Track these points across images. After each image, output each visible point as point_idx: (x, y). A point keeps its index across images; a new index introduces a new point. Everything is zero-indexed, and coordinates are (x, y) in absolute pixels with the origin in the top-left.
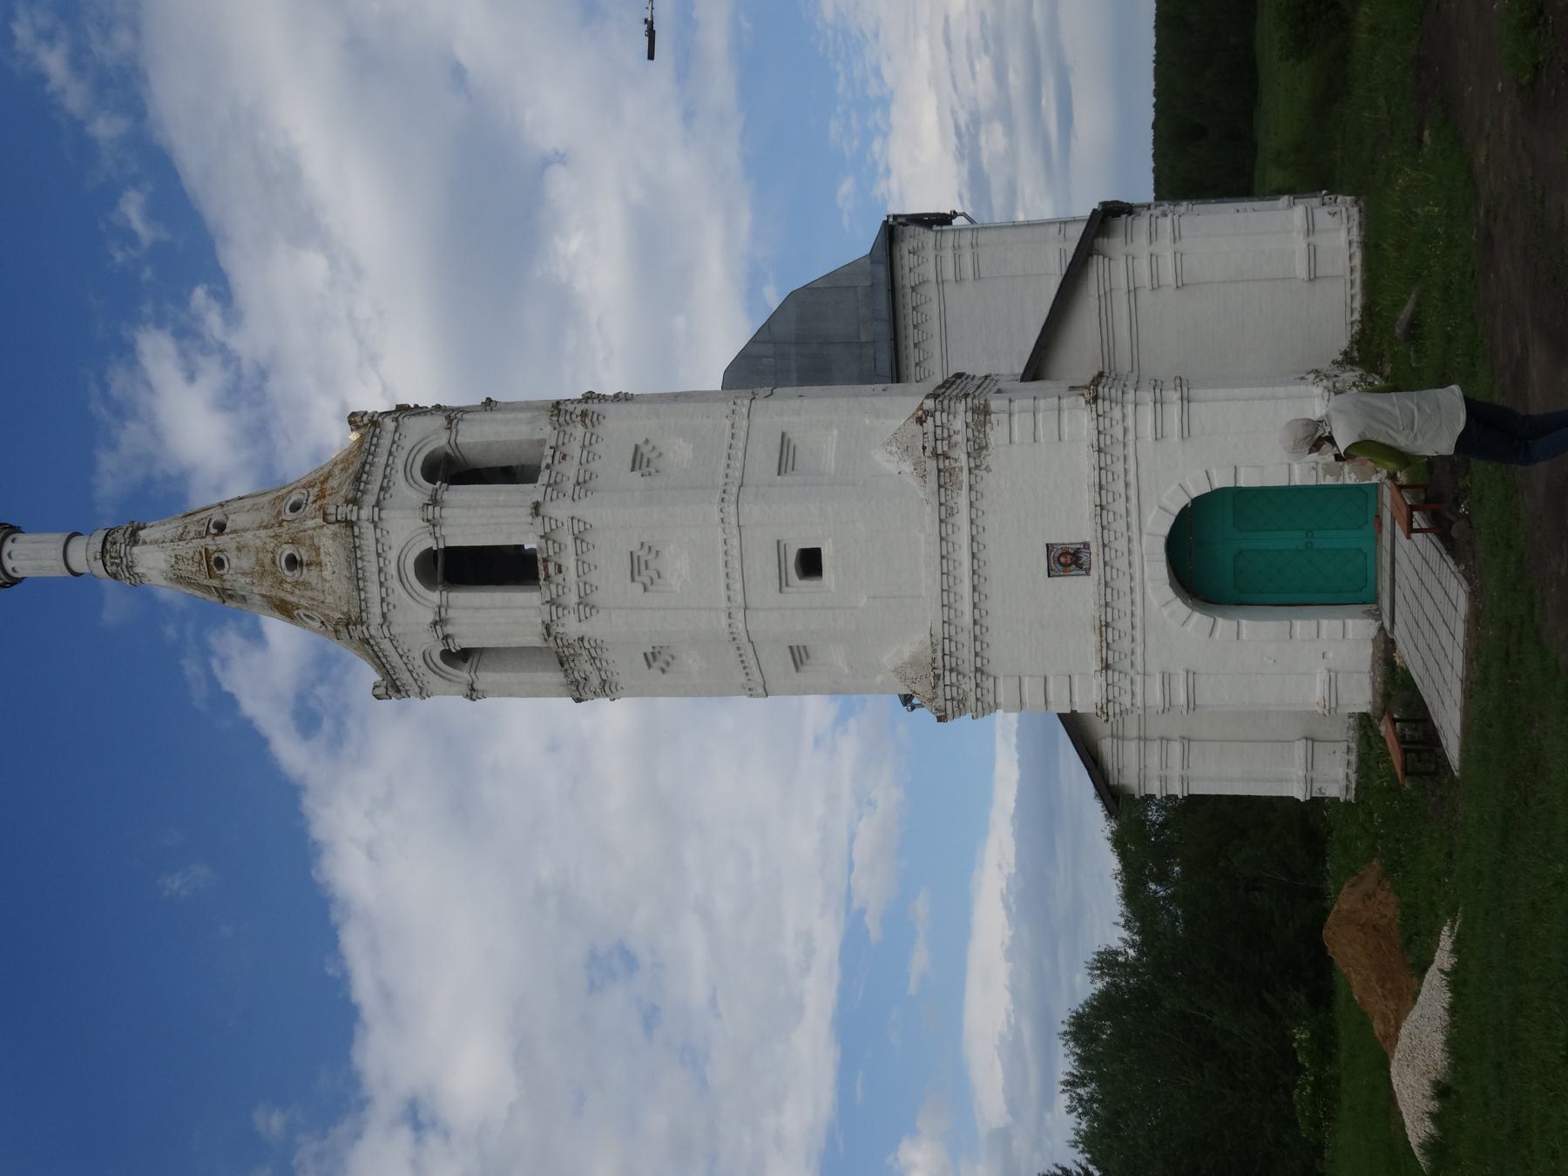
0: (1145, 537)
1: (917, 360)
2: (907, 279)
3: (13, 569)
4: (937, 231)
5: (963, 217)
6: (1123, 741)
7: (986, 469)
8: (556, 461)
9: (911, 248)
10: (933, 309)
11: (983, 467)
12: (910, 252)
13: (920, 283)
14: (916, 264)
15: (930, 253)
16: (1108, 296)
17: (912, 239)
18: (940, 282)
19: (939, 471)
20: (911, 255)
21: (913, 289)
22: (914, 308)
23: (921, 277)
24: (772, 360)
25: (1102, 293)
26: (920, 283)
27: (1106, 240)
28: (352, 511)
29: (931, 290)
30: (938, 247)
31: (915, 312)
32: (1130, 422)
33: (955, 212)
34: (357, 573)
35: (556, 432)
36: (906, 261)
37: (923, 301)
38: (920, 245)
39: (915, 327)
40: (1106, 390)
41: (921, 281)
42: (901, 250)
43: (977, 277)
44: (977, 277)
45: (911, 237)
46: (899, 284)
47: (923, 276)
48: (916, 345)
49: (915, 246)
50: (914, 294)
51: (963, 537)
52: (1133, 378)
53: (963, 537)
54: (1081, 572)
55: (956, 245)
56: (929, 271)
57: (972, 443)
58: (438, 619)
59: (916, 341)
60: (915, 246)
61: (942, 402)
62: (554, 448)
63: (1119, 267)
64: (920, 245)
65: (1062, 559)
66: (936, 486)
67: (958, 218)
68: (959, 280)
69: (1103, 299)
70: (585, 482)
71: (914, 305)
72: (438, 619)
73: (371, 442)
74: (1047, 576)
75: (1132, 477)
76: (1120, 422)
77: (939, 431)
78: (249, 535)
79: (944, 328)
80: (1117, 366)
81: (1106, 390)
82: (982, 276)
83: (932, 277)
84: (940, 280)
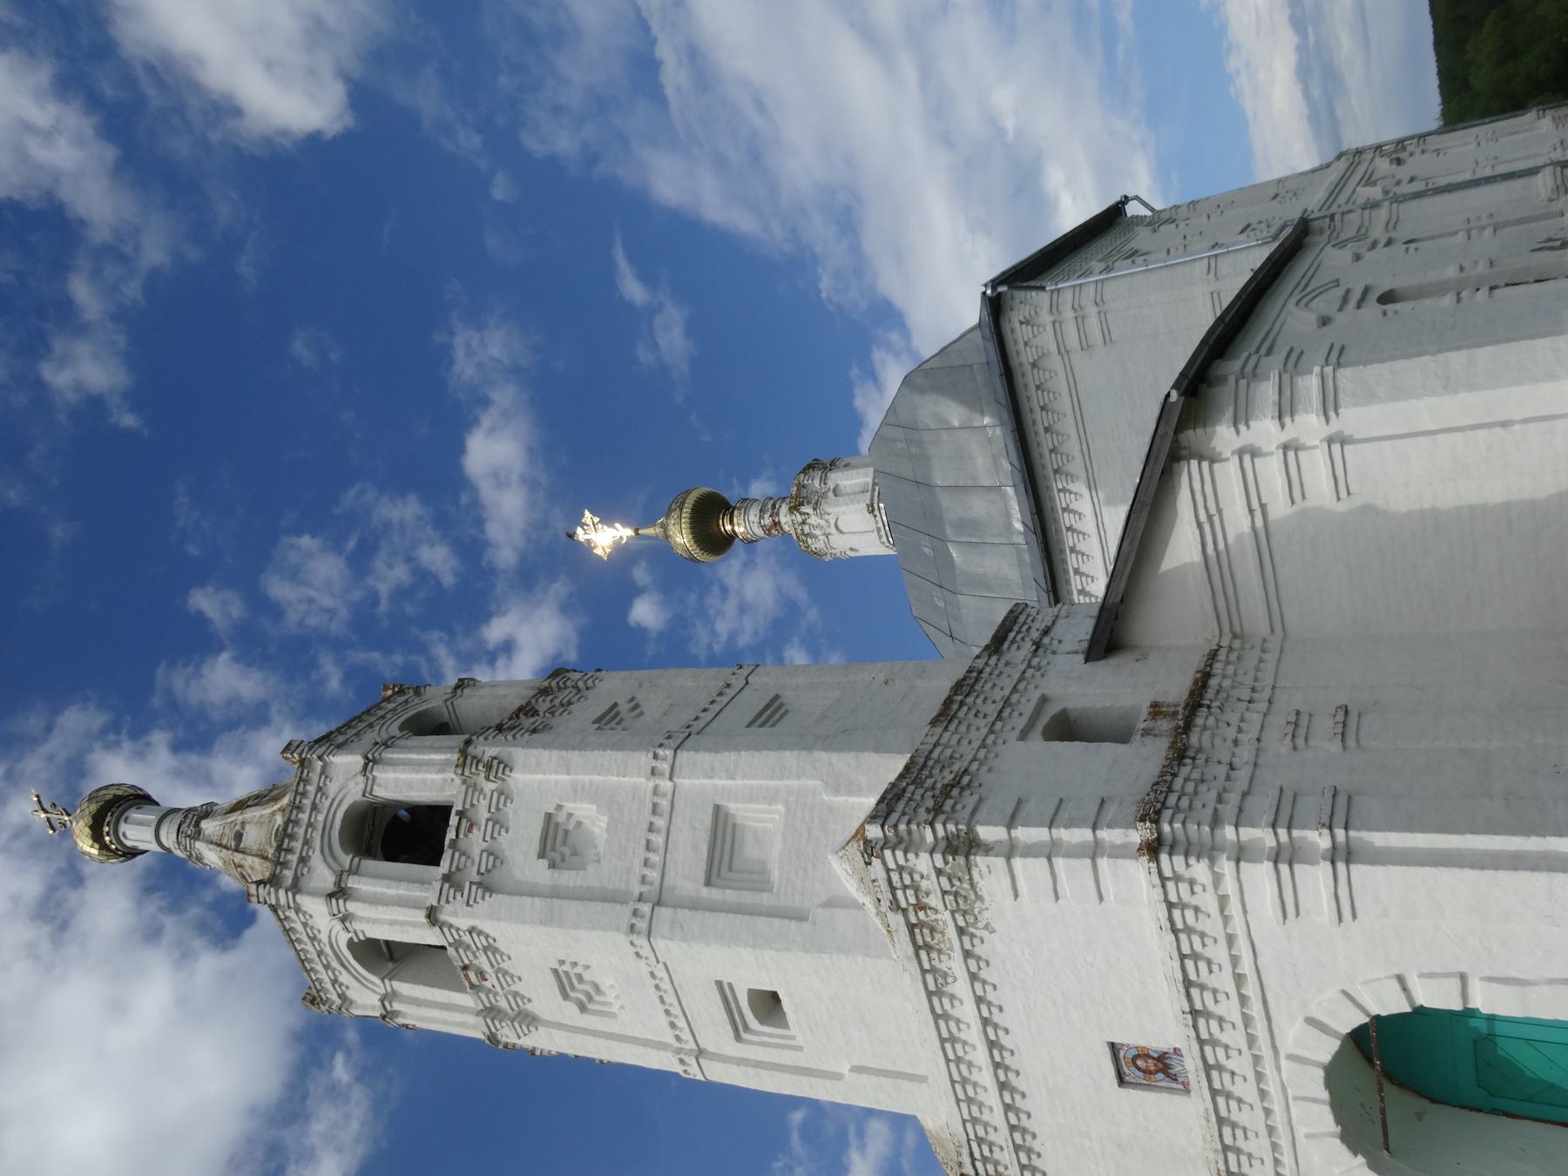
0: (1283, 1062)
1: (1051, 447)
2: (1023, 357)
3: (124, 835)
4: (1052, 291)
5: (1135, 202)
6: (1348, 862)
7: (986, 927)
8: (461, 836)
9: (1022, 318)
10: (1060, 384)
11: (980, 925)
12: (1021, 323)
13: (1039, 357)
14: (1031, 336)
15: (1046, 318)
16: (1216, 520)
17: (1023, 305)
18: (1064, 352)
19: (911, 928)
20: (1024, 326)
21: (1034, 365)
22: (1038, 387)
23: (1039, 350)
24: (904, 444)
25: (1203, 517)
26: (1039, 357)
27: (1200, 431)
28: (269, 893)
29: (1055, 362)
30: (1054, 308)
31: (1039, 392)
32: (1229, 886)
33: (1126, 197)
34: (299, 955)
35: (464, 787)
36: (1018, 335)
37: (1047, 377)
38: (1033, 313)
39: (1043, 408)
40: (1177, 825)
41: (1040, 354)
42: (1010, 322)
43: (1107, 339)
44: (1107, 339)
45: (1021, 303)
46: (1014, 362)
47: (1042, 349)
48: (1047, 430)
49: (1027, 315)
50: (1035, 371)
51: (967, 1011)
52: (1274, 644)
53: (967, 1011)
54: (1174, 1085)
55: (1076, 306)
56: (1047, 340)
57: (952, 898)
58: (385, 1013)
59: (1046, 425)
60: (1027, 315)
61: (895, 826)
62: (461, 814)
63: (1229, 472)
64: (1033, 313)
65: (1140, 1063)
66: (910, 949)
67: (1130, 203)
68: (1086, 346)
69: (1213, 510)
70: (488, 871)
71: (1038, 383)
72: (385, 1013)
73: (296, 791)
74: (1115, 1082)
75: (1246, 967)
76: (1210, 888)
77: (895, 877)
78: (250, 859)
79: (1078, 408)
80: (1246, 626)
81: (1177, 825)
82: (1113, 339)
83: (1053, 347)
84: (1063, 351)
